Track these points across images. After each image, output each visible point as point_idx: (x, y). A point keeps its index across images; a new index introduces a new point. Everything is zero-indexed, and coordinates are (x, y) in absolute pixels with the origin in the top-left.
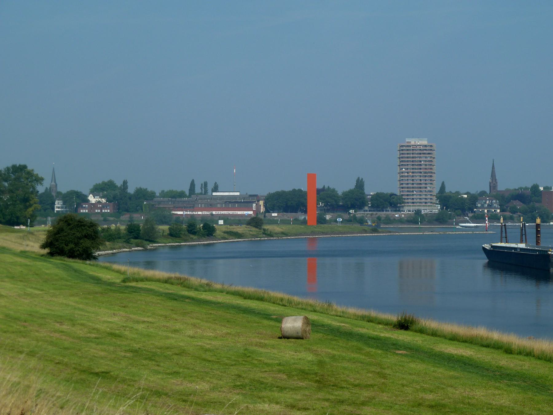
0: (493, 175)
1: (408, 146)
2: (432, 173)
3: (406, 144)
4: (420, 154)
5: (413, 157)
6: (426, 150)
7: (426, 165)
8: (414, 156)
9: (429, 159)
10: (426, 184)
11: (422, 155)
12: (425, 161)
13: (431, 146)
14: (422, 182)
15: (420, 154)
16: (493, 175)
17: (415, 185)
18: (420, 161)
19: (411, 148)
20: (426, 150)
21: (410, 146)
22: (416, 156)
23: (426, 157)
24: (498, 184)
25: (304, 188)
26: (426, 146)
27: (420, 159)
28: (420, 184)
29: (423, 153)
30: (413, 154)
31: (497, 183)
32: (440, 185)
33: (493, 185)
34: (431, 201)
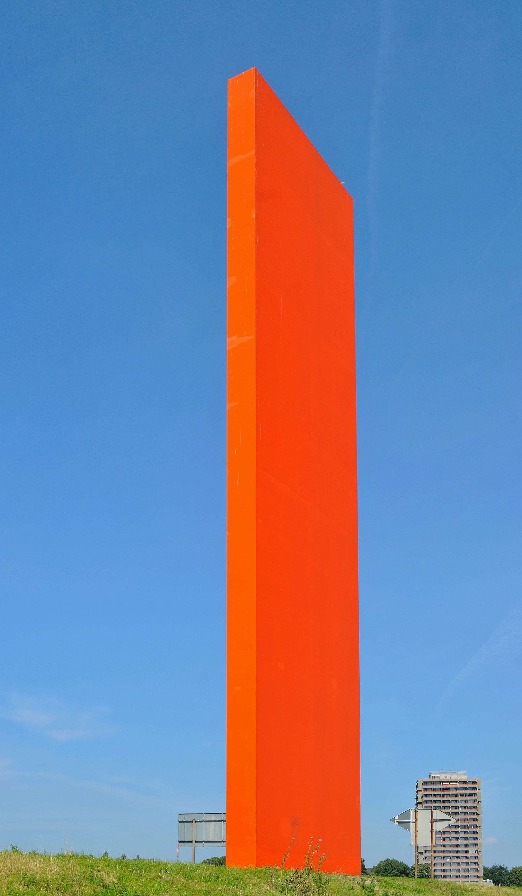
6: (465, 789)
7: (466, 814)
9: (470, 804)
12: (465, 807)
13: (475, 782)
20: (465, 789)
23: (466, 801)
26: (465, 782)
29: (462, 795)
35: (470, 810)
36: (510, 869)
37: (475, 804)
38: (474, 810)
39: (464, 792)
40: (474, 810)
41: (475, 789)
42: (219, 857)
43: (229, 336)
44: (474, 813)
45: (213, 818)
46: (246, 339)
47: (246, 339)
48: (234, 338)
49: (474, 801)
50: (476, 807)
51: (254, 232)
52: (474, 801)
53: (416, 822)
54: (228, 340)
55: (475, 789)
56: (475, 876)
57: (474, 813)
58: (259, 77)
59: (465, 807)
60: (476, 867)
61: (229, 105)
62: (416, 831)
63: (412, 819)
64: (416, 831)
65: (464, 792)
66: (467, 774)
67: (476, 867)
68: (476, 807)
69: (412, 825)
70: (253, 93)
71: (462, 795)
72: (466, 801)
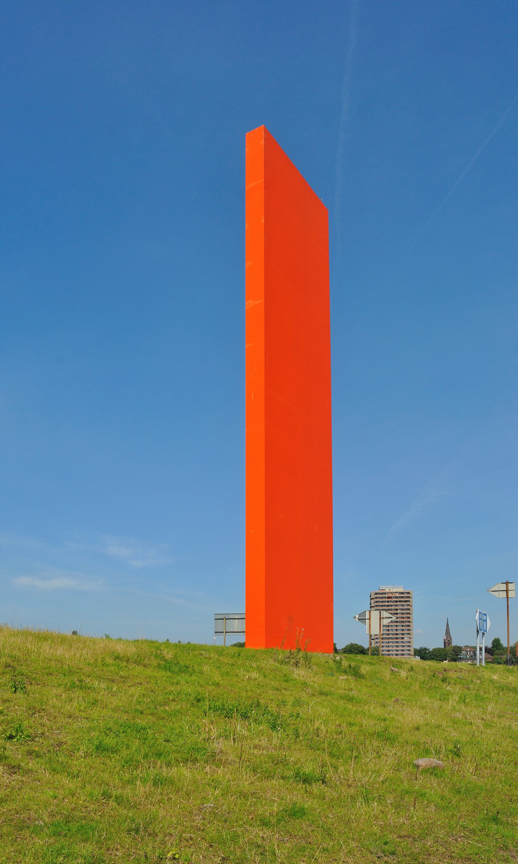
0: (448, 632)
1: (382, 593)
2: (409, 622)
3: (381, 592)
4: (396, 602)
5: (388, 606)
6: (402, 597)
7: (403, 614)
8: (389, 604)
9: (406, 607)
10: (403, 634)
11: (398, 603)
12: (402, 609)
13: (409, 593)
14: (398, 632)
15: (396, 602)
16: (448, 632)
17: (390, 636)
18: (397, 610)
19: (387, 596)
20: (402, 597)
21: (385, 593)
22: (391, 604)
23: (403, 605)
24: (453, 640)
25: (366, 648)
26: (402, 593)
27: (397, 608)
28: (397, 634)
29: (400, 601)
30: (388, 602)
31: (451, 639)
32: (235, 648)
33: (448, 642)
34: (409, 653)
35: (405, 612)
36: (431, 650)
38: (408, 612)
39: (401, 599)
40: (408, 612)
46: (258, 302)
47: (258, 302)
48: (250, 301)
49: (408, 605)
50: (409, 609)
51: (263, 232)
52: (408, 605)
53: (370, 619)
59: (402, 609)
60: (409, 648)
61: (246, 150)
62: (370, 624)
63: (367, 617)
64: (370, 624)
65: (401, 599)
67: (409, 648)
68: (409, 609)
69: (367, 621)
70: (262, 142)
71: (400, 601)
72: (403, 605)
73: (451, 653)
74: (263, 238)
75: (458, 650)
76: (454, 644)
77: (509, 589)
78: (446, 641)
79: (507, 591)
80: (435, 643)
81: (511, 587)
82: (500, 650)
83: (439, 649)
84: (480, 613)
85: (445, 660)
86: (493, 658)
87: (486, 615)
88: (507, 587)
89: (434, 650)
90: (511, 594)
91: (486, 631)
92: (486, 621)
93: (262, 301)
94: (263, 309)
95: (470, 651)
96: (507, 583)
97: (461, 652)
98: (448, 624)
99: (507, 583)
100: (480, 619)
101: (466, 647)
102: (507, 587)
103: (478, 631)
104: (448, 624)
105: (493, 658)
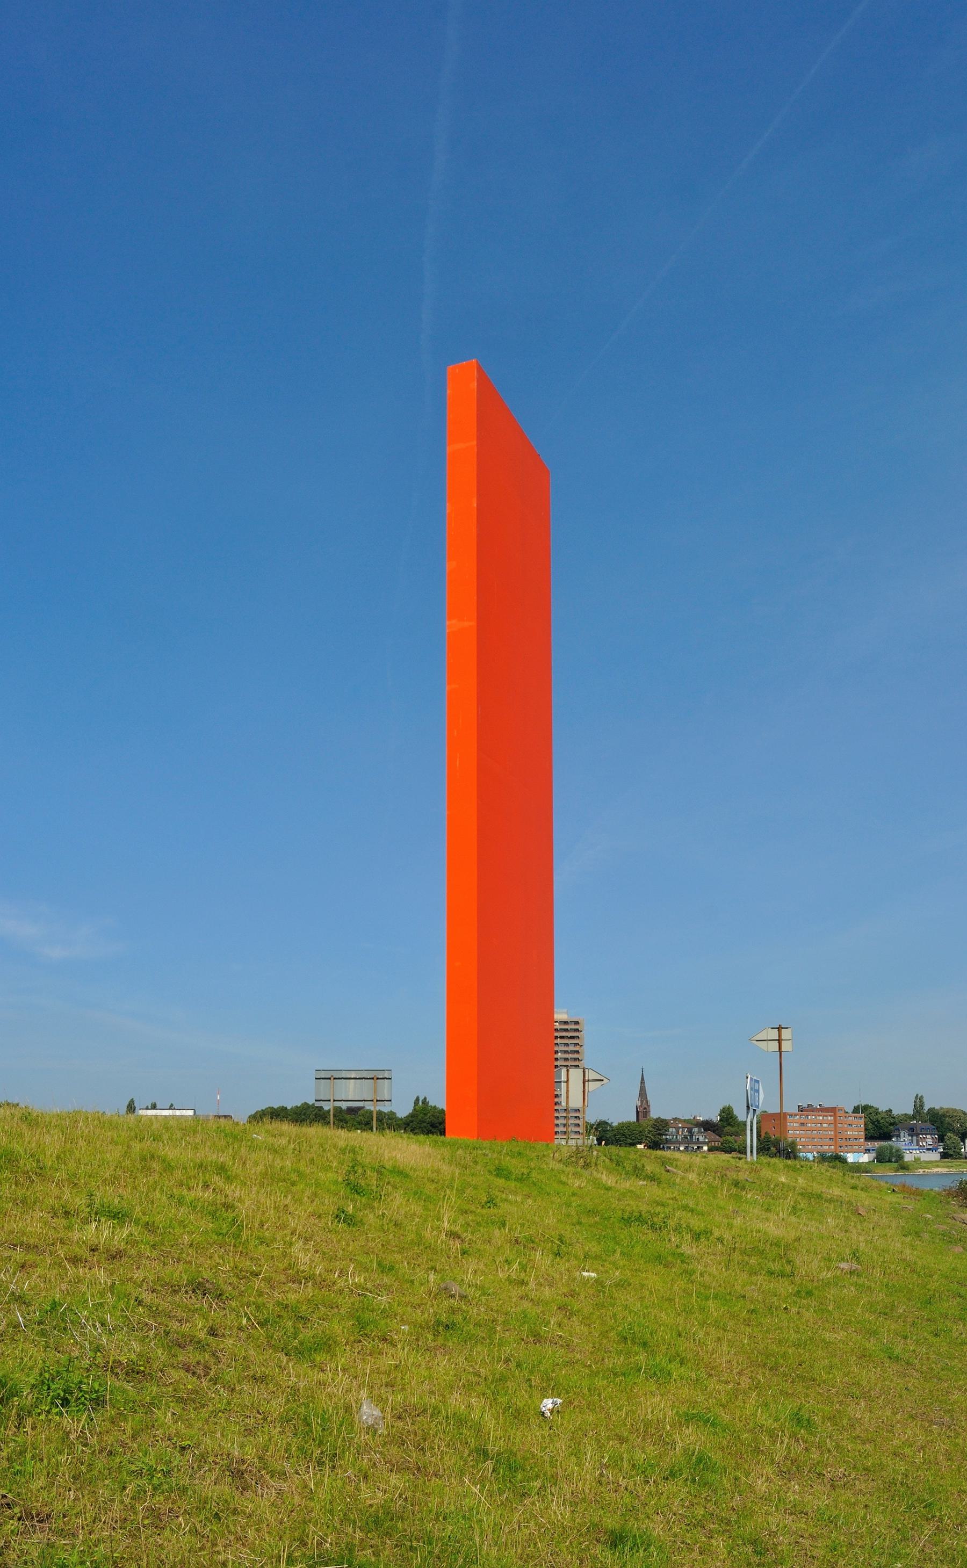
0: (643, 1094)
6: (566, 1030)
7: (566, 1059)
9: (572, 1048)
12: (565, 1052)
13: (577, 1023)
16: (643, 1094)
20: (566, 1030)
23: (567, 1045)
26: (566, 1023)
29: (562, 1037)
33: (642, 1111)
35: (571, 1056)
36: (615, 1124)
37: (577, 1048)
38: (576, 1056)
39: (564, 1034)
40: (576, 1056)
41: (577, 1030)
42: (276, 1107)
43: (449, 619)
44: (575, 1059)
45: (365, 1075)
46: (466, 624)
47: (466, 624)
48: (454, 622)
49: (576, 1044)
50: (578, 1052)
51: (475, 521)
52: (576, 1044)
53: (567, 1082)
54: (447, 623)
55: (577, 1030)
56: (576, 1132)
57: (575, 1059)
58: (479, 369)
59: (565, 1052)
60: (577, 1122)
61: (448, 392)
62: (568, 1091)
63: (564, 1078)
64: (568, 1091)
65: (564, 1034)
66: (567, 1013)
67: (577, 1122)
68: (578, 1052)
69: (563, 1085)
70: (474, 385)
71: (562, 1037)
72: (567, 1045)
73: (650, 1134)
74: (474, 530)
75: (661, 1126)
76: (654, 1114)
77: (783, 1037)
78: (640, 1109)
79: (779, 1041)
80: (621, 1113)
81: (786, 1034)
82: (733, 1126)
83: (628, 1125)
84: (751, 1079)
85: (640, 1143)
86: (721, 1140)
87: (757, 1082)
88: (780, 1035)
89: (622, 1125)
90: (786, 1046)
91: (758, 1107)
92: (758, 1091)
93: (473, 623)
94: (554, 710)
95: (683, 1128)
96: (779, 1029)
97: (668, 1130)
98: (643, 1079)
99: (779, 1029)
100: (751, 1089)
101: (675, 1119)
102: (780, 1035)
103: (748, 1107)
104: (643, 1079)
105: (721, 1140)
